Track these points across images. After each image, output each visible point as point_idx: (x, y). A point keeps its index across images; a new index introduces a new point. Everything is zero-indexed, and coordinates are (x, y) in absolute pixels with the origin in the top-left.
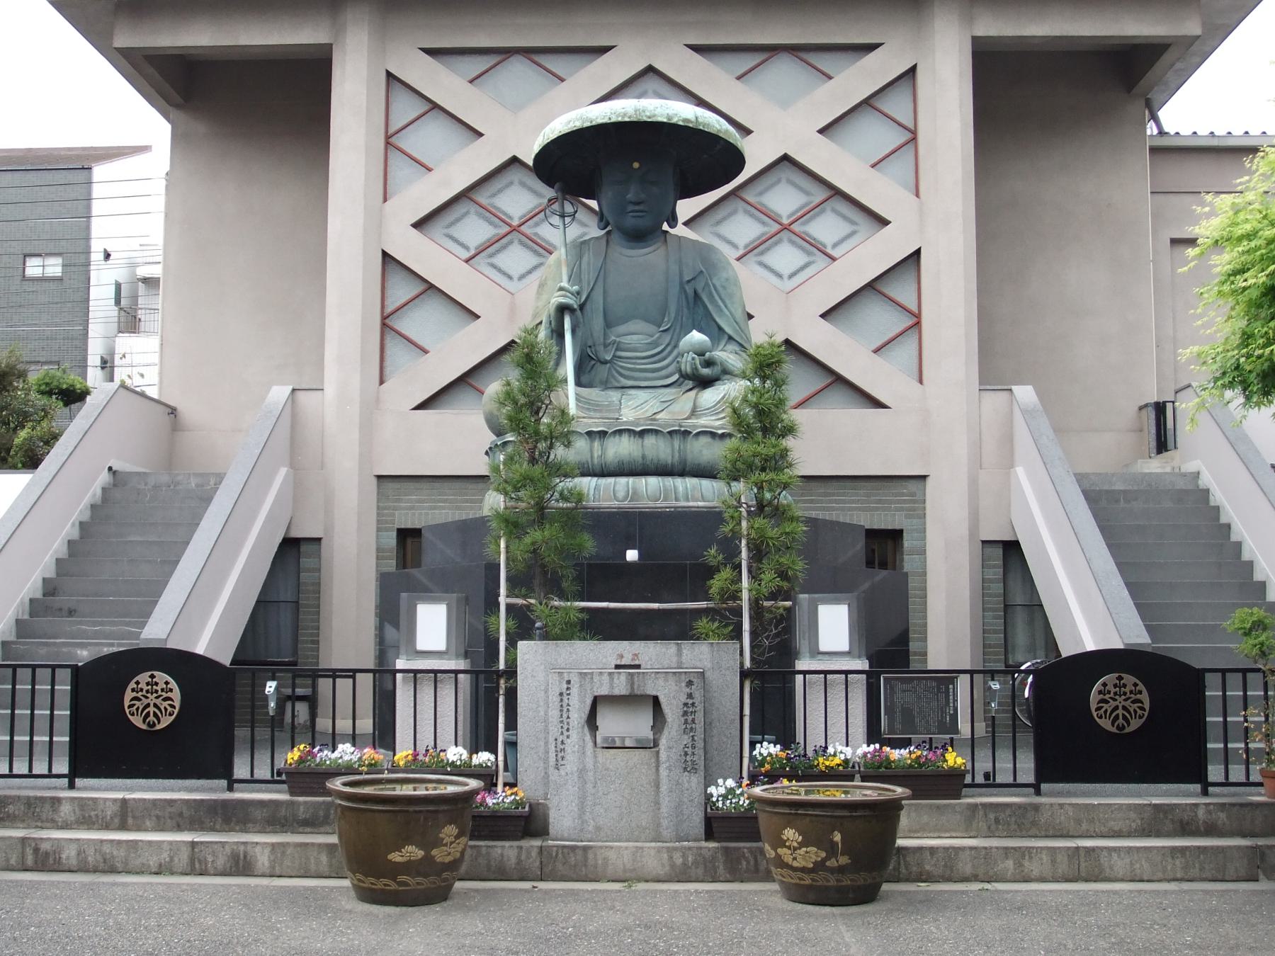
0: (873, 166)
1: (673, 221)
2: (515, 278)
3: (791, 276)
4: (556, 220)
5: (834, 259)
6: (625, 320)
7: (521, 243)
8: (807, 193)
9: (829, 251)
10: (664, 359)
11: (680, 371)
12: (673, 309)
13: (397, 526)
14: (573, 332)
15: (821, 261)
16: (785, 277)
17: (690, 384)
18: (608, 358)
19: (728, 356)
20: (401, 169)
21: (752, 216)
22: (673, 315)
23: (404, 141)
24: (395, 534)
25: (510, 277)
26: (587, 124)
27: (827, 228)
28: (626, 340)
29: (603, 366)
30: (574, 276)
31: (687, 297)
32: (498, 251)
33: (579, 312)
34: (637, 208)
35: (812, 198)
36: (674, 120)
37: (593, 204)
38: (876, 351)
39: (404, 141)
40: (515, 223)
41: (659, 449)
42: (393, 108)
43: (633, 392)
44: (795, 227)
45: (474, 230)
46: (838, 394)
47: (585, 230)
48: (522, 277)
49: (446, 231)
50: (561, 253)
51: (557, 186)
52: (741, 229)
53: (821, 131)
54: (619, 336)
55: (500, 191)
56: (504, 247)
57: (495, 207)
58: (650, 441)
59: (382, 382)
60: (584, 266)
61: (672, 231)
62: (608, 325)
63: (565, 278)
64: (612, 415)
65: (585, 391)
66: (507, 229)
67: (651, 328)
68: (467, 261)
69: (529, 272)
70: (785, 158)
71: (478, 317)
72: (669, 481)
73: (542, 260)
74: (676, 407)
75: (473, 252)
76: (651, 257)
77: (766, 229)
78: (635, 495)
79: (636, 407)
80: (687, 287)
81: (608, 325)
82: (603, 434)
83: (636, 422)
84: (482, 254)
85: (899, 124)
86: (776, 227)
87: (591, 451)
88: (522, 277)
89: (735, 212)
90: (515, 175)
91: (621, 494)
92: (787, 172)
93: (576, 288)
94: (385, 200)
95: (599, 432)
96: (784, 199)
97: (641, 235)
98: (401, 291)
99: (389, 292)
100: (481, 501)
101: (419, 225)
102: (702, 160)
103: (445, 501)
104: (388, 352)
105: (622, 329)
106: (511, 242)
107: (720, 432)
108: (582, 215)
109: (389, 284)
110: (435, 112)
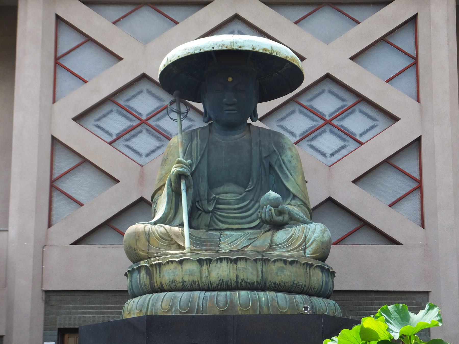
0: (388, 81)
1: (254, 116)
2: (328, 155)
3: (332, 155)
4: (174, 115)
5: (361, 144)
6: (221, 184)
7: (148, 132)
8: (342, 100)
9: (358, 138)
10: (249, 210)
11: (261, 217)
12: (254, 175)
13: (58, 326)
14: (187, 191)
15: (352, 145)
16: (328, 155)
17: (268, 227)
18: (211, 209)
19: (293, 208)
20: (65, 80)
21: (305, 115)
22: (255, 181)
23: (68, 62)
24: (56, 332)
25: (140, 155)
26: (198, 51)
27: (356, 123)
28: (224, 197)
29: (207, 215)
30: (187, 153)
31: (264, 168)
32: (133, 137)
33: (190, 178)
34: (230, 108)
35: (345, 103)
36: (257, 50)
37: (200, 106)
38: (391, 205)
39: (68, 62)
40: (144, 118)
41: (249, 273)
42: (60, 40)
43: (227, 232)
44: (151, 122)
45: (116, 123)
46: (364, 235)
47: (192, 123)
48: (148, 155)
49: (96, 123)
50: (177, 140)
51: (175, 93)
52: (298, 123)
53: (352, 58)
54: (217, 194)
55: (134, 96)
56: (137, 134)
57: (130, 107)
58: (241, 265)
59: (50, 226)
60: (194, 146)
61: (253, 123)
62: (211, 186)
63: (181, 154)
64: (213, 248)
65: (195, 232)
66: (138, 122)
67: (240, 189)
68: (110, 143)
69: (153, 151)
70: (328, 77)
71: (118, 181)
72: (255, 294)
73: (162, 143)
74: (258, 243)
75: (114, 137)
76: (237, 137)
77: (315, 123)
78: (293, 306)
79: (231, 241)
80: (264, 162)
81: (211, 186)
82: (209, 261)
83: (232, 252)
84: (122, 139)
85: (406, 54)
86: (322, 122)
87: (201, 273)
88: (148, 155)
89: (293, 112)
90: (144, 86)
91: (221, 303)
92: (329, 86)
93: (189, 161)
94: (54, 102)
95: (206, 260)
96: (327, 104)
97: (231, 126)
98: (64, 163)
99: (56, 164)
100: (122, 307)
101: (78, 119)
102: (275, 76)
103: (92, 308)
104: (55, 205)
105: (221, 189)
106: (141, 131)
107: (290, 260)
108: (191, 114)
109: (56, 158)
110: (89, 44)
